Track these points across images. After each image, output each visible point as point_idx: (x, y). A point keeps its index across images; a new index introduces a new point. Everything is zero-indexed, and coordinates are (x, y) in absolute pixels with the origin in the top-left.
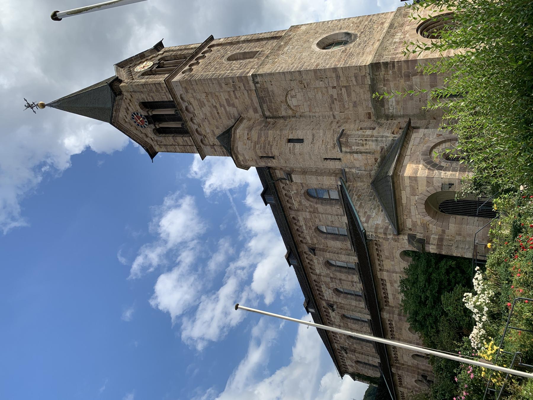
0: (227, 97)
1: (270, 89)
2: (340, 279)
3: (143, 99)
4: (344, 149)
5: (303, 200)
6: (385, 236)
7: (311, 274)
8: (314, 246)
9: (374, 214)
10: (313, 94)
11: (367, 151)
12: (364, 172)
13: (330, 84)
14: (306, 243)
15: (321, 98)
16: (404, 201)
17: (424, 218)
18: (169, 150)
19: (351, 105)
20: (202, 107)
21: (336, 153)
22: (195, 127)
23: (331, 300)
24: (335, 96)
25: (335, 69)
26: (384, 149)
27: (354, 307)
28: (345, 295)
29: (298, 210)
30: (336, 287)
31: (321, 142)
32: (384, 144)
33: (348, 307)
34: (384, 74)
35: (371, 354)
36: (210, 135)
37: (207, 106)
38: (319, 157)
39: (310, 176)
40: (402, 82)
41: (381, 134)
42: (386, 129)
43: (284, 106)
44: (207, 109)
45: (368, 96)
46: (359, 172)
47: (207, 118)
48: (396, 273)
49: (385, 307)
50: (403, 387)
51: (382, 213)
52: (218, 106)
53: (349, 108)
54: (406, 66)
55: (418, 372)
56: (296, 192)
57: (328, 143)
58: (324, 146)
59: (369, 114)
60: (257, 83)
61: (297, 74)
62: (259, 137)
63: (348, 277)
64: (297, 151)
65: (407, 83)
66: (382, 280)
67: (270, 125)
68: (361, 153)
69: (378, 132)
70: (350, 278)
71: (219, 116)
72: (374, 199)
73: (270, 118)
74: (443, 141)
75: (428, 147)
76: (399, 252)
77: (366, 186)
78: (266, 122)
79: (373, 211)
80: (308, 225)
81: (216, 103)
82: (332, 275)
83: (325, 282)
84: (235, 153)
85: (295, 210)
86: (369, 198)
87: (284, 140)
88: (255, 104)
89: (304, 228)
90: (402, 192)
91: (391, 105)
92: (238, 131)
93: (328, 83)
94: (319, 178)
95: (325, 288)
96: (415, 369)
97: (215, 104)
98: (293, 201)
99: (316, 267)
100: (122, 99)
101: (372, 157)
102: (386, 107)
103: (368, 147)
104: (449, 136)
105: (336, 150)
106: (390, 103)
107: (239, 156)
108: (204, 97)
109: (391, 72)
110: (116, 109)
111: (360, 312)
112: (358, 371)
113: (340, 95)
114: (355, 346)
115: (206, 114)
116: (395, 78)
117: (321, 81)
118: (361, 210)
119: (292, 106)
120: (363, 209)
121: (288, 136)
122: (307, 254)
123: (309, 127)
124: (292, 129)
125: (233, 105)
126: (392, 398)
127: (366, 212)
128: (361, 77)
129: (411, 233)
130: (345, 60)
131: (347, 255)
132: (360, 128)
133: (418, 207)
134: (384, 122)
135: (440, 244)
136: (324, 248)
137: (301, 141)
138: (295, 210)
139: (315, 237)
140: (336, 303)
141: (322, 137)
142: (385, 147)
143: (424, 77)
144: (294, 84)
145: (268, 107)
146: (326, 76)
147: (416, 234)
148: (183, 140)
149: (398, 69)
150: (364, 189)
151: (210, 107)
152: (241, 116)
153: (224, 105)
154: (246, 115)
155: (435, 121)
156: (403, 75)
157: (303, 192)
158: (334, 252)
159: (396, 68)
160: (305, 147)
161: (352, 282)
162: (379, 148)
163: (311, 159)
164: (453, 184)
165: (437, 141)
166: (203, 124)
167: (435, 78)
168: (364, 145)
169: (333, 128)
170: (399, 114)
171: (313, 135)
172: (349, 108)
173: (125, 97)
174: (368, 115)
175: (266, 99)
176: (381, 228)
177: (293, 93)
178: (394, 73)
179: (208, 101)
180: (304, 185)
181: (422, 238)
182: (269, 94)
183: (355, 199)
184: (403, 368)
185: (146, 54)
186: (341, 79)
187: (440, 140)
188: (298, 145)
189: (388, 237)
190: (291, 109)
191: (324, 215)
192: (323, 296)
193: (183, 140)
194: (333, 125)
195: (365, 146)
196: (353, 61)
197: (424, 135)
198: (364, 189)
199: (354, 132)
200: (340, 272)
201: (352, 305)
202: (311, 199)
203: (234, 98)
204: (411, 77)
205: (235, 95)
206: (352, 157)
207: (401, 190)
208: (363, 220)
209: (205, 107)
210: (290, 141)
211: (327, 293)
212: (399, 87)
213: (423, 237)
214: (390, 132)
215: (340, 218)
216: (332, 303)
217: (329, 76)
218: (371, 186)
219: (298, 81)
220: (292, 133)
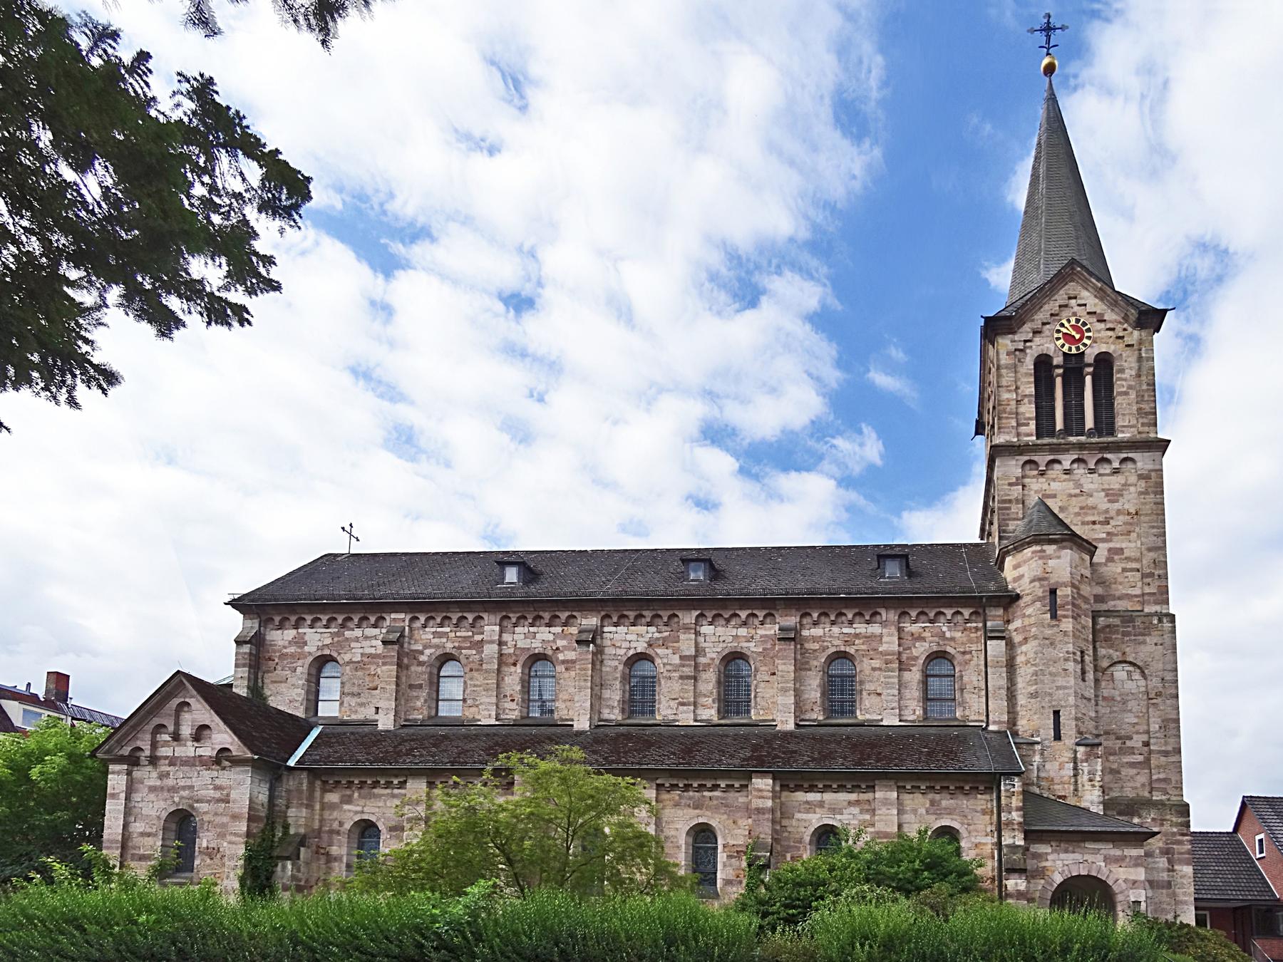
0: (1127, 553)
1: (1148, 639)
3: (1122, 371)
5: (927, 645)
11: (1080, 786)
15: (1127, 720)
19: (1115, 766)
20: (1107, 495)
24: (1129, 743)
25: (1178, 751)
34: (1172, 821)
36: (1045, 486)
37: (1109, 505)
38: (1063, 703)
39: (1004, 675)
43: (1116, 655)
44: (1100, 501)
46: (1035, 767)
47: (1082, 495)
52: (1108, 528)
53: (1108, 761)
54: (1183, 851)
60: (1160, 621)
61: (1173, 691)
68: (1075, 775)
71: (1087, 523)
81: (1115, 526)
88: (1113, 603)
89: (846, 630)
93: (1157, 738)
98: (923, 625)
100: (1126, 318)
107: (1054, 547)
108: (1126, 506)
109: (1175, 830)
110: (1105, 292)
113: (1132, 751)
115: (1091, 496)
117: (1160, 727)
119: (1112, 669)
143: (1166, 873)
144: (1155, 683)
145: (1115, 626)
149: (1179, 840)
151: (1107, 511)
153: (1111, 541)
159: (1180, 838)
163: (1058, 688)
166: (1070, 480)
172: (1108, 761)
173: (1130, 329)
175: (1129, 627)
177: (1137, 676)
178: (1174, 834)
179: (1119, 512)
180: (968, 657)
182: (1139, 635)
186: (1163, 759)
190: (1111, 666)
191: (896, 680)
195: (1090, 783)
201: (601, 689)
203: (1124, 565)
205: (1132, 570)
209: (1106, 499)
219: (1161, 689)
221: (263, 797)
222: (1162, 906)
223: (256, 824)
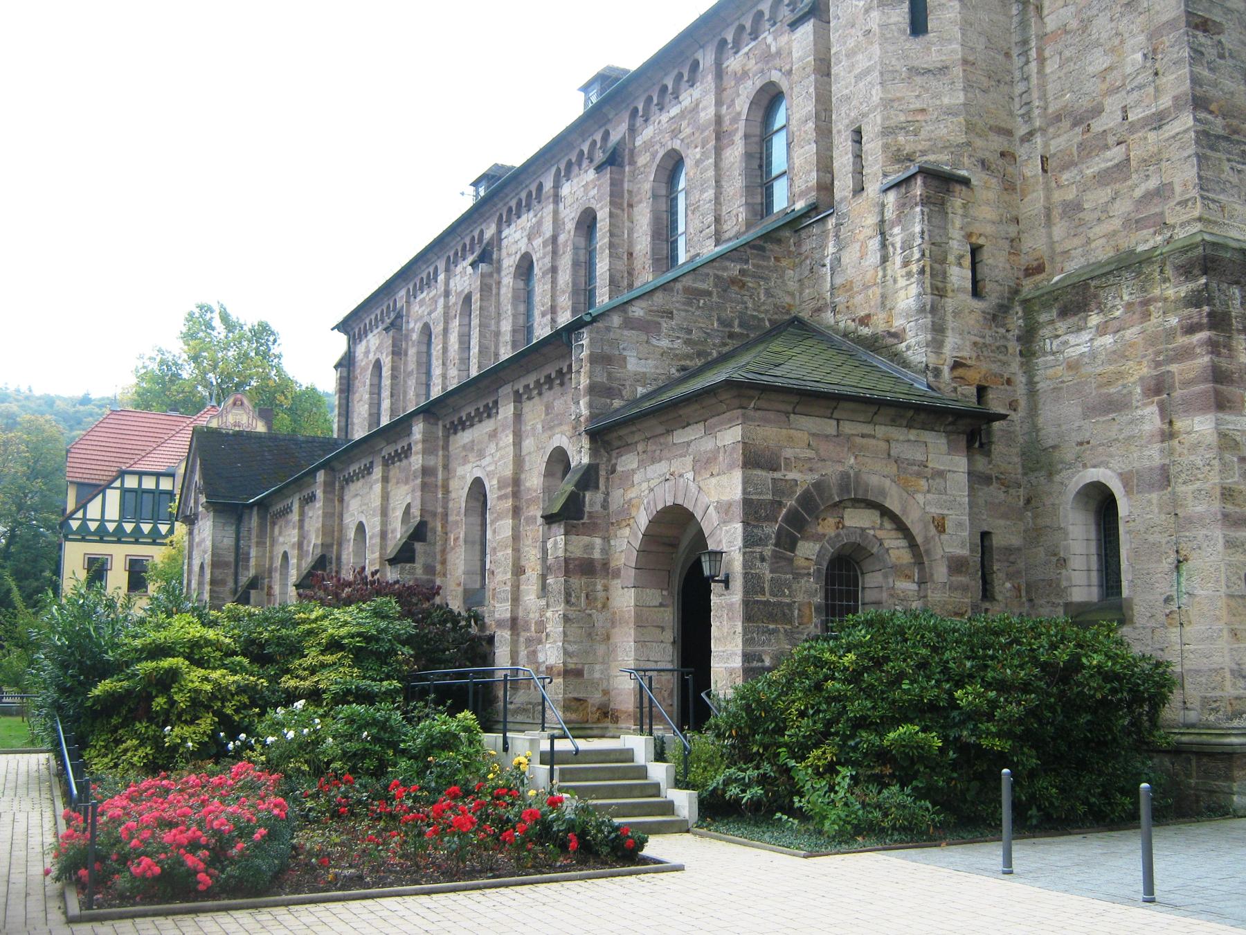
4: (891, 197)
6: (582, 393)
7: (554, 170)
9: (665, 343)
10: (1104, 36)
12: (829, 285)
13: (1135, 94)
17: (642, 508)
23: (504, 252)
24: (1097, 126)
26: (896, 341)
27: (493, 328)
28: (522, 294)
29: (719, 74)
31: (918, 105)
32: (913, 340)
33: (492, 309)
34: (1166, 300)
40: (1140, 370)
41: (950, 323)
42: (978, 339)
45: (1099, 251)
48: (514, 444)
49: (440, 423)
50: (302, 508)
51: (673, 371)
55: (332, 545)
56: (773, 49)
58: (902, 119)
59: (1039, 266)
63: (564, 292)
65: (1139, 390)
66: (496, 403)
69: (961, 312)
72: (731, 336)
74: (913, 538)
75: (883, 493)
77: (788, 299)
79: (678, 338)
80: (684, 123)
83: (540, 223)
86: (732, 320)
90: (701, 426)
91: (1066, 343)
93: (1140, 87)
95: (529, 225)
96: (336, 533)
101: (872, 304)
102: (1062, 326)
103: (902, 282)
104: (938, 557)
105: (889, 169)
106: (1072, 339)
112: (361, 374)
116: (1152, 341)
117: (1145, 55)
120: (684, 304)
123: (980, 47)
127: (669, 314)
128: (1157, 210)
129: (602, 473)
130: (1235, 137)
132: (981, 241)
133: (667, 484)
134: (1011, 327)
135: (571, 566)
136: (626, 195)
139: (654, 156)
140: (499, 270)
141: (938, 102)
142: (904, 344)
146: (1160, 73)
147: (597, 487)
150: (772, 296)
155: (1021, 503)
156: (1164, 369)
157: (775, 76)
158: (616, 231)
162: (898, 323)
164: (727, 587)
165: (913, 520)
167: (1151, 487)
168: (908, 269)
169: (979, 143)
170: (1040, 375)
171: (944, 69)
174: (1035, 264)
176: (609, 374)
178: (1170, 334)
181: (587, 509)
183: (725, 269)
184: (333, 501)
186: (1152, 136)
187: (916, 530)
189: (581, 402)
194: (993, 137)
196: (1227, 168)
197: (940, 474)
198: (772, 296)
199: (958, 223)
202: (759, 116)
204: (1156, 399)
206: (869, 232)
207: (705, 421)
208: (634, 309)
212: (1124, 361)
213: (589, 513)
214: (965, 354)
215: (708, 230)
216: (495, 256)
217: (1163, 80)
218: (787, 317)
221: (228, 542)
222: (1151, 539)
223: (221, 570)
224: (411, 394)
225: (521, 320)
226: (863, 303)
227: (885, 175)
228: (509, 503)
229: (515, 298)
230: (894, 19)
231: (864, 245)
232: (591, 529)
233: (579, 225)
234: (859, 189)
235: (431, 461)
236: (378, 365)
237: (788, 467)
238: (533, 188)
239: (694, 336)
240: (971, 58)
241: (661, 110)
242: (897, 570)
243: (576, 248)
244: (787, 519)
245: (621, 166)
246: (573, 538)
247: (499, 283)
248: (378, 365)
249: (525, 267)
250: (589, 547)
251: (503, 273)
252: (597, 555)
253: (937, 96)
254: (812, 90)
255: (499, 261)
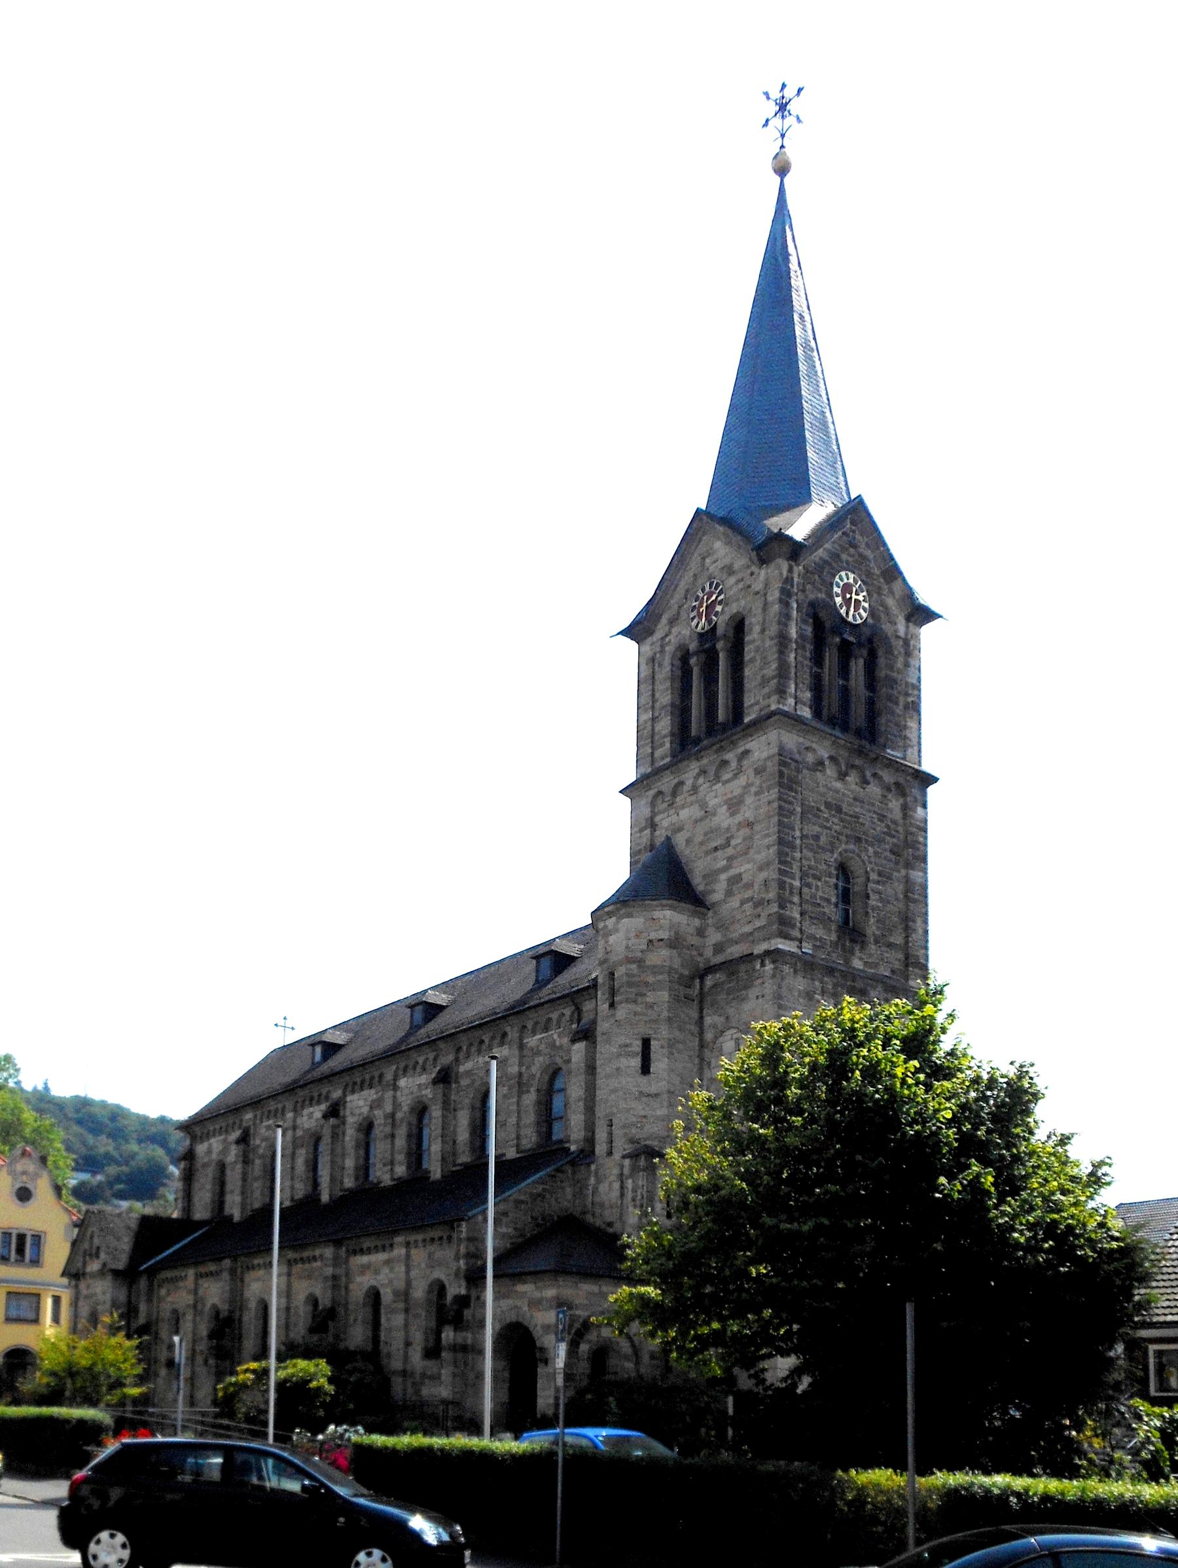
2: (393, 1136)
5: (541, 1059)
7: (394, 1067)
8: (453, 1081)
14: (457, 1060)
16: (521, 1288)
18: (641, 686)
21: (621, 1146)
22: (689, 777)
30: (376, 1123)
31: (642, 1113)
35: (248, 1201)
36: (674, 818)
44: (723, 819)
52: (730, 851)
57: (642, 1128)
58: (634, 1120)
62: (655, 970)
64: (624, 1062)
66: (391, 1245)
67: (683, 991)
70: (400, 1157)
72: (538, 1225)
73: (701, 989)
76: (443, 1277)
78: (692, 978)
82: (399, 1115)
84: (618, 910)
85: (521, 1039)
87: (644, 1030)
92: (668, 913)
94: (581, 1104)
97: (733, 842)
99: (410, 1080)
103: (631, 1209)
105: (626, 1147)
107: (614, 919)
111: (333, 1179)
114: (258, 1162)
118: (511, 1205)
121: (655, 1039)
122: (435, 1059)
124: (671, 1044)
125: (729, 893)
126: (164, 1254)
131: (442, 1155)
137: (645, 1069)
138: (521, 1039)
139: (473, 1081)
140: (344, 1123)
148: (665, 736)
151: (728, 829)
152: (709, 909)
154: (710, 921)
157: (558, 1060)
160: (633, 1080)
161: (392, 1163)
171: (657, 1095)
185: (897, 586)
188: (636, 1062)
192: (353, 1092)
193: (665, 736)
200: (409, 1136)
209: (728, 814)
210: (646, 1043)
211: (361, 1103)
216: (342, 1114)
220: (662, 1047)
224: (257, 1194)
225: (361, 1161)
226: (610, 1215)
227: (624, 1150)
228: (401, 1305)
229: (357, 1146)
230: (633, 1064)
231: (610, 1184)
232: (466, 1328)
233: (412, 1110)
234: (610, 1153)
235: (338, 1271)
236: (222, 1167)
237: (577, 1308)
238: (376, 1074)
239: (519, 1226)
240: (672, 1089)
241: (479, 1054)
242: (626, 1358)
243: (410, 1124)
244: (575, 1334)
245: (449, 1083)
246: (458, 1334)
247: (344, 1133)
248: (222, 1167)
249: (367, 1127)
250: (465, 1339)
251: (348, 1126)
252: (469, 1341)
253: (654, 1110)
254: (583, 1083)
255: (344, 1117)
